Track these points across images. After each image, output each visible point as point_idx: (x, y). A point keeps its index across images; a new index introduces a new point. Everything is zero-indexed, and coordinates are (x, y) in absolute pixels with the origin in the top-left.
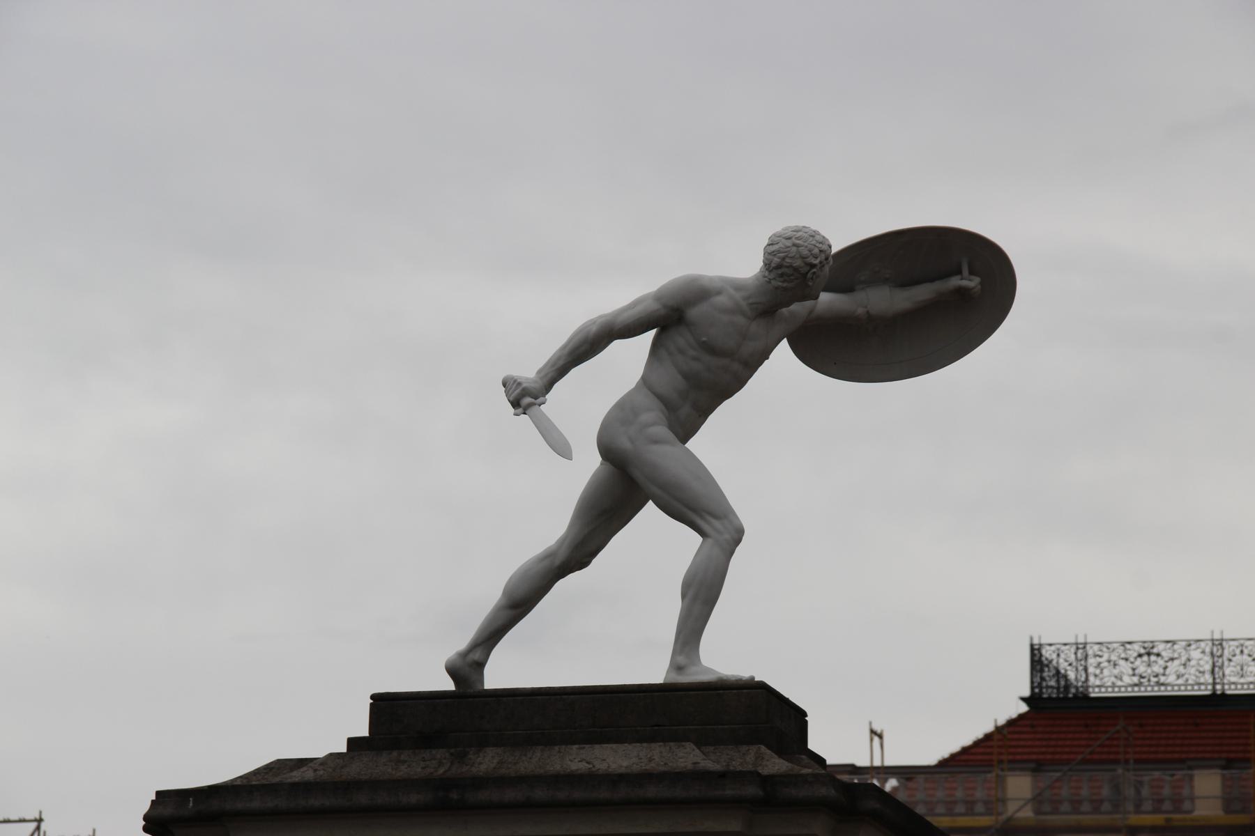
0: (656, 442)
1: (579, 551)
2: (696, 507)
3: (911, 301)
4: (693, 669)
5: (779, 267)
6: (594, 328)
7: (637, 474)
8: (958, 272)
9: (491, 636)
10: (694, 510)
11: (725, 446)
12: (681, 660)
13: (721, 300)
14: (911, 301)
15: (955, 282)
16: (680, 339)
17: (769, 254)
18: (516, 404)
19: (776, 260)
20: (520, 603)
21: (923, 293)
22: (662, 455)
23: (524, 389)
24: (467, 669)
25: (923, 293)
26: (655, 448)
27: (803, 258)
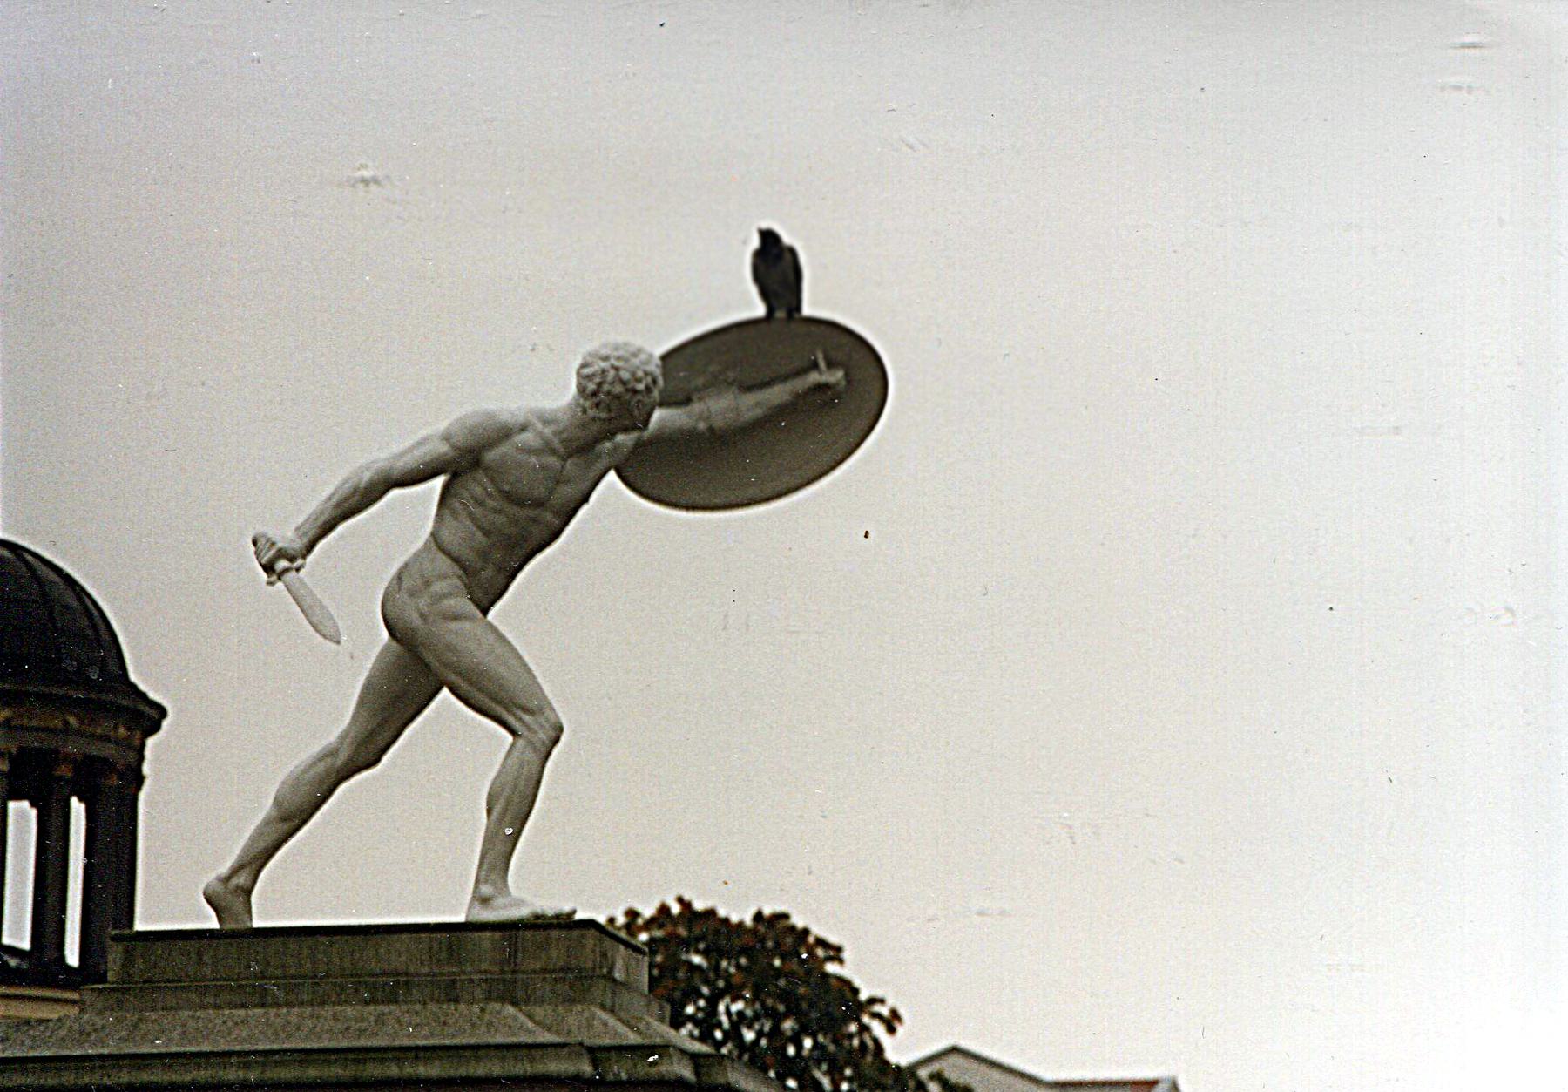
0: (456, 617)
1: (368, 746)
2: (499, 698)
3: (769, 398)
4: (500, 901)
5: (595, 394)
6: (367, 476)
7: (429, 657)
8: (815, 366)
9: (257, 859)
10: (499, 702)
11: (534, 616)
12: (486, 890)
13: (527, 438)
14: (769, 398)
15: (814, 377)
16: (477, 485)
17: (583, 378)
18: (268, 568)
19: (591, 386)
20: (293, 815)
21: (778, 394)
22: (464, 636)
23: (280, 550)
24: (231, 894)
25: (778, 394)
26: (454, 625)
27: (624, 383)
